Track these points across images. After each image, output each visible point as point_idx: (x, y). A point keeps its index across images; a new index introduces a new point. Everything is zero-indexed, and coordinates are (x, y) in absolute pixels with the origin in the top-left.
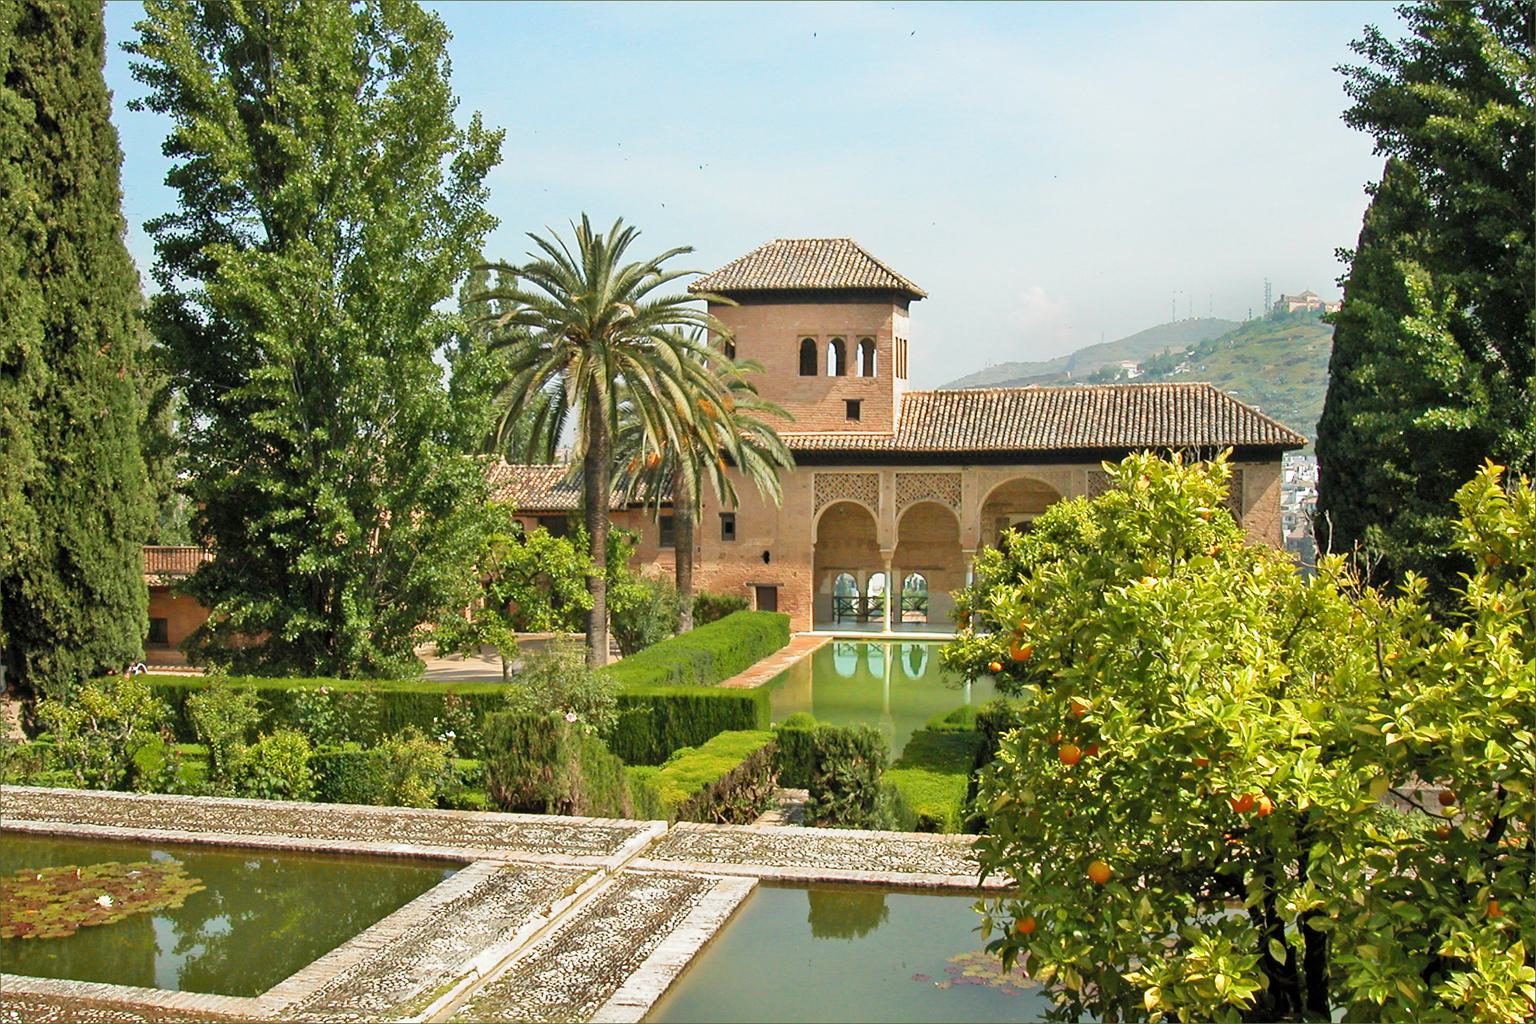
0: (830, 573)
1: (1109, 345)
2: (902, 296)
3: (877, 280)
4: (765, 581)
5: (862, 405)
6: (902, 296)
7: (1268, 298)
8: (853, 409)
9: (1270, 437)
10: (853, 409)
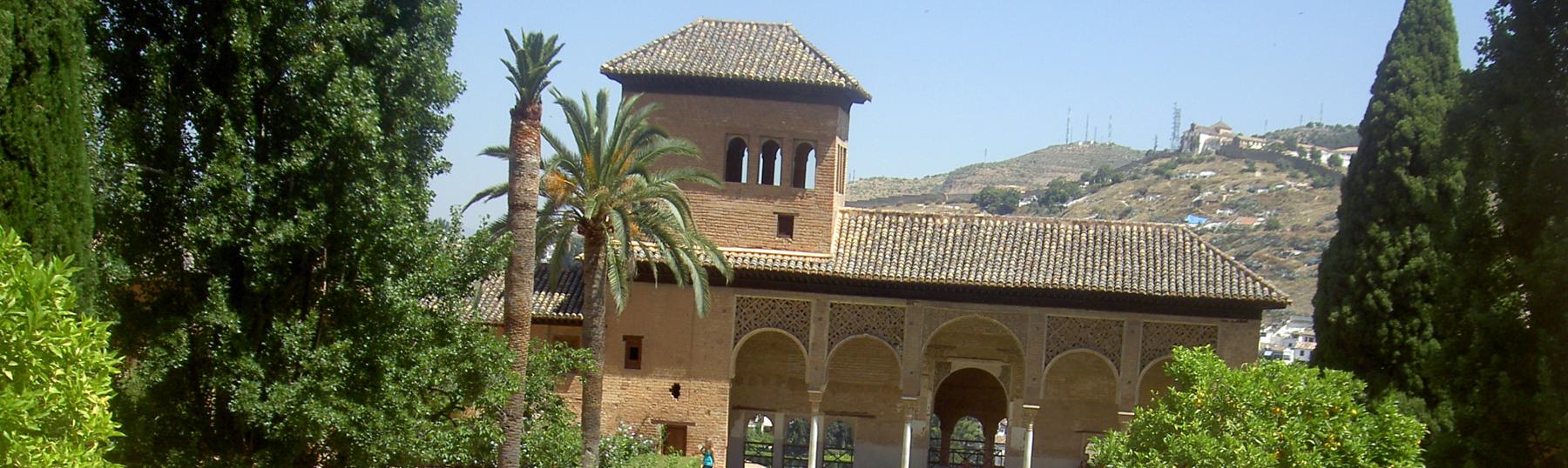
0: (743, 413)
1: (992, 166)
2: (861, 98)
3: (822, 77)
4: (674, 418)
5: (796, 221)
6: (861, 98)
7: (1176, 126)
8: (786, 226)
9: (1250, 290)
10: (786, 226)
